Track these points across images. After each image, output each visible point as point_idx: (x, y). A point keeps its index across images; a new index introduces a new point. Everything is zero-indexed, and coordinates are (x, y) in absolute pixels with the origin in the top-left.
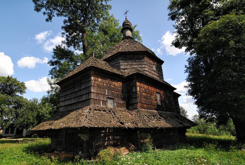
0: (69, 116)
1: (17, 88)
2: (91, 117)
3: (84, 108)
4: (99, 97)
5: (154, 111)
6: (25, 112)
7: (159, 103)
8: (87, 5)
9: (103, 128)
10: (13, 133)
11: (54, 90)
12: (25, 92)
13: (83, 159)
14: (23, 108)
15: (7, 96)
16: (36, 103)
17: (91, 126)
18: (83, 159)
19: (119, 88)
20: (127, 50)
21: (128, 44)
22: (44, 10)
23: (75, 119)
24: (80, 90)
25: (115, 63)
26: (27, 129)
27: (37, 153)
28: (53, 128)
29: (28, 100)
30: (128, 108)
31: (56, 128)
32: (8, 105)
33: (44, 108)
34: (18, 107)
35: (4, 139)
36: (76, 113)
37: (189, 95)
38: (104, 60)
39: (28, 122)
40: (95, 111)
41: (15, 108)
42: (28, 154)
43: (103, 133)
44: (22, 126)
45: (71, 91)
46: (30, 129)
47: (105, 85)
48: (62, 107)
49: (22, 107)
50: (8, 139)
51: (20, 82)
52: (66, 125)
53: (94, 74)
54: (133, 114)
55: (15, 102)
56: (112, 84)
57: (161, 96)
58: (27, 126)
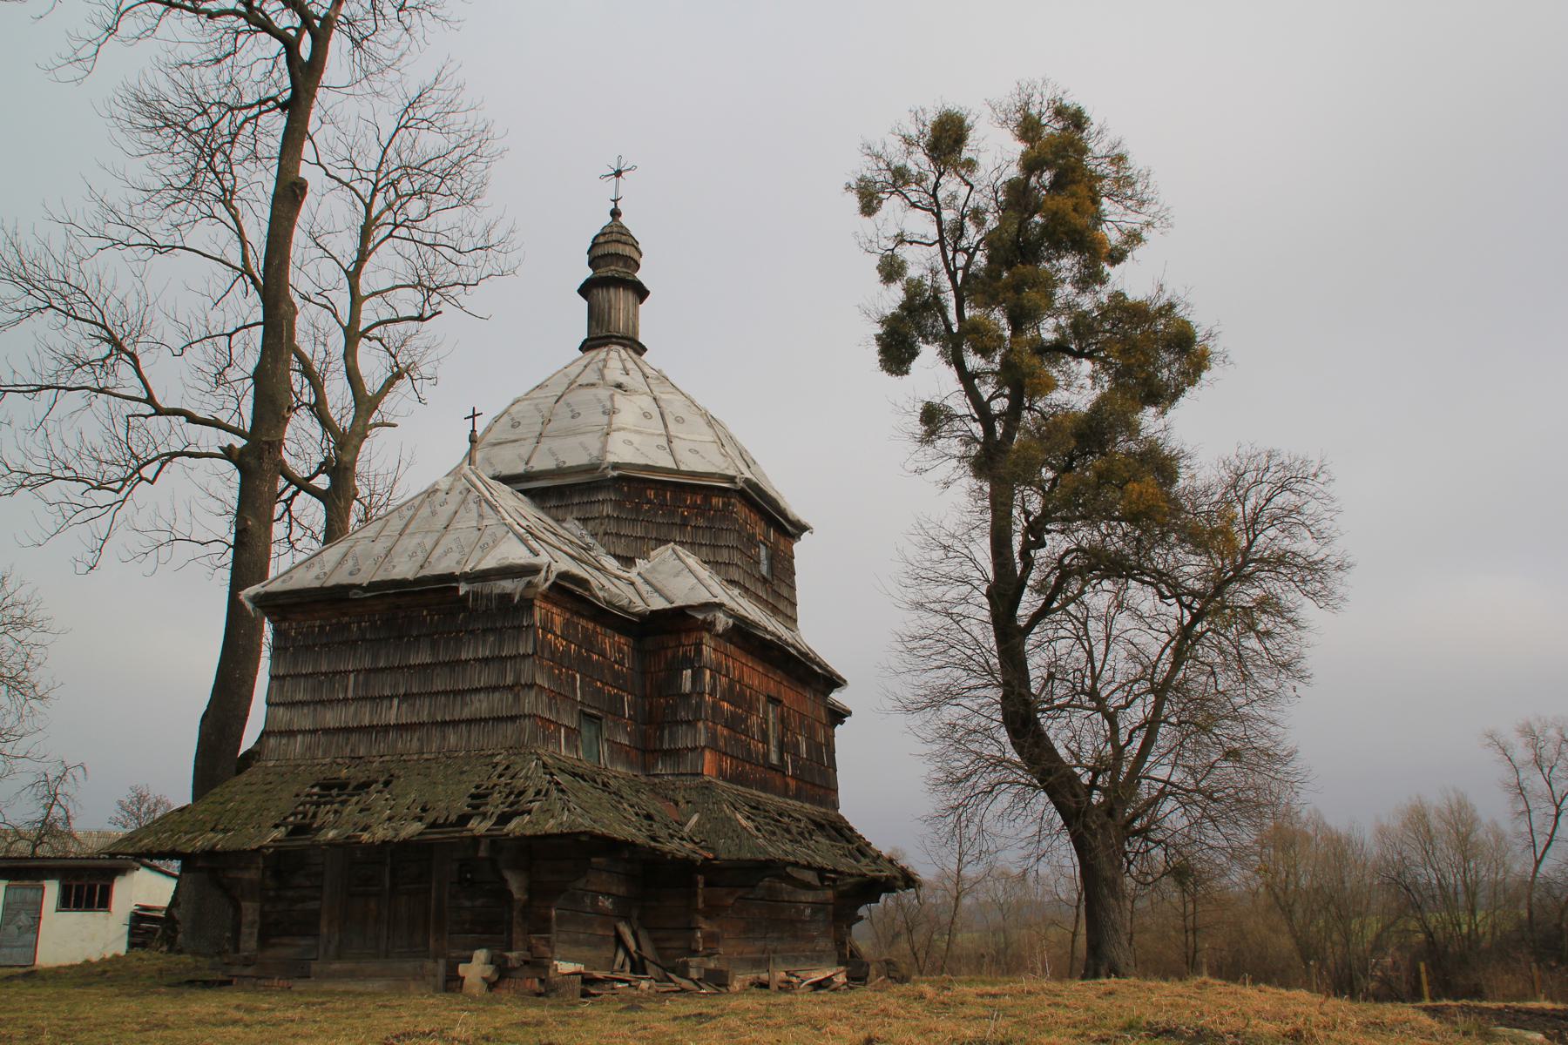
4: (558, 712)
19: (616, 666)
24: (455, 665)
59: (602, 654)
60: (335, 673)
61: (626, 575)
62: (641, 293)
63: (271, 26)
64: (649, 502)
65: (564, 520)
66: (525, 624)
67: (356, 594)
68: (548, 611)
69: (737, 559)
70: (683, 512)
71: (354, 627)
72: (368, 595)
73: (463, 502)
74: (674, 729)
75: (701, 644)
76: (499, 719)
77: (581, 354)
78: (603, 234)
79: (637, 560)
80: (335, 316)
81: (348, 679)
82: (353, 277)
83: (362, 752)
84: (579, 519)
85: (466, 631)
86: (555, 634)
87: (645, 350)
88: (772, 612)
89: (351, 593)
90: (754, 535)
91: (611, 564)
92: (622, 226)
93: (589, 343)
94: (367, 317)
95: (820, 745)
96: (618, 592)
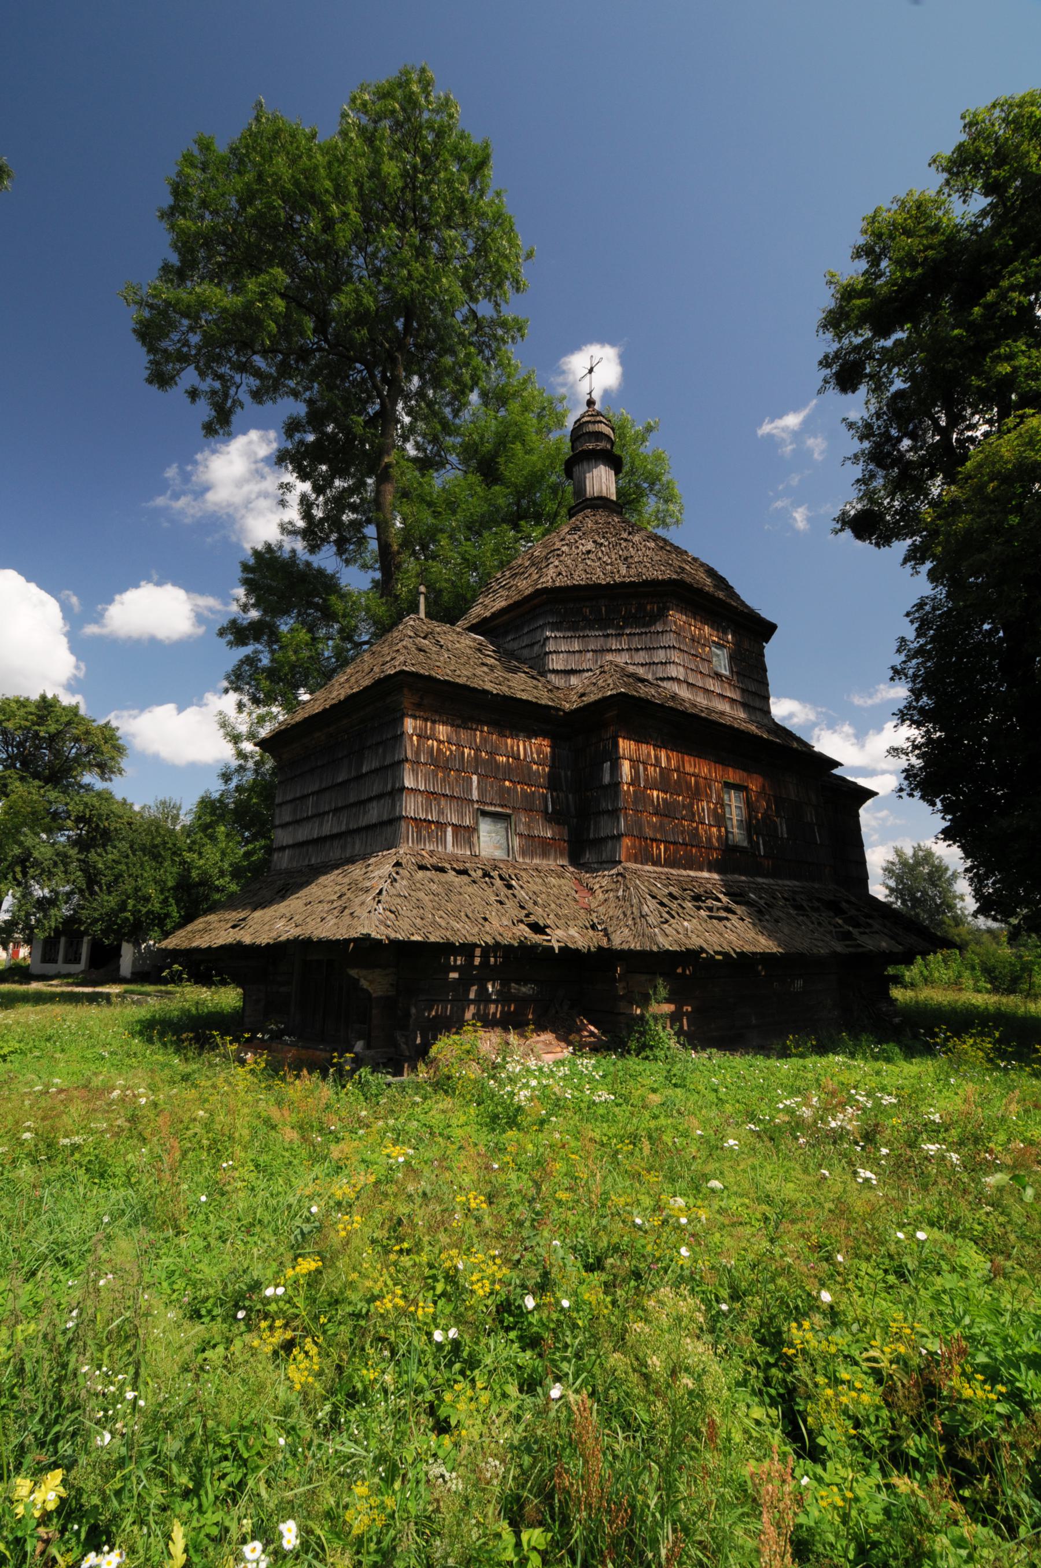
0: (313, 891)
1: (84, 750)
2: (398, 900)
3: (372, 860)
4: (441, 812)
5: (706, 874)
6: (127, 864)
7: (737, 834)
8: (400, 324)
9: (447, 948)
10: (77, 960)
11: (250, 764)
12: (120, 771)
13: (368, 1069)
14: (115, 847)
15: (40, 787)
16: (174, 823)
17: (393, 935)
18: (368, 1069)
19: (535, 767)
20: (580, 578)
21: (590, 546)
22: (189, 377)
23: (335, 904)
24: (360, 777)
25: (526, 641)
26: (137, 944)
27: (186, 1039)
28: (247, 940)
29: (137, 808)
30: (576, 859)
31: (258, 941)
32: (49, 831)
33: (208, 849)
34: (94, 838)
35: (35, 986)
36: (339, 879)
37: (911, 795)
38: (473, 628)
39: (140, 911)
40: (420, 874)
41: (82, 844)
42: (153, 1043)
43: (455, 968)
44: (114, 931)
46: (151, 942)
48: (282, 849)
49: (110, 840)
50: (56, 987)
51: (95, 724)
52: (298, 929)
53: (419, 706)
54: (596, 886)
55: (79, 819)
56: (503, 750)
57: (749, 804)
58: (136, 932)
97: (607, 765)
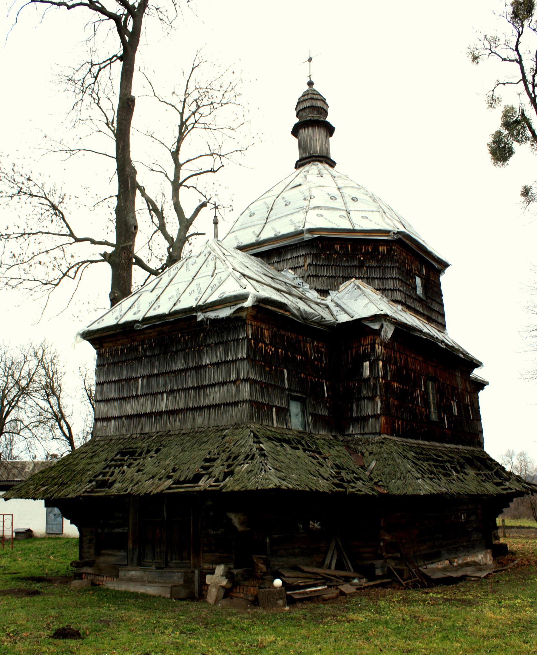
4: (270, 397)
24: (199, 368)
45: (152, 367)
47: (282, 353)
59: (305, 354)
60: (131, 379)
61: (323, 302)
62: (330, 130)
63: (104, 10)
64: (336, 252)
65: (282, 270)
66: (241, 337)
67: (138, 326)
68: (258, 328)
69: (398, 284)
70: (360, 258)
71: (140, 348)
72: (145, 326)
73: (206, 261)
74: (360, 403)
75: (375, 343)
76: (227, 405)
77: (295, 170)
78: (303, 96)
79: (330, 292)
80: (166, 176)
81: (138, 382)
82: (175, 154)
83: (147, 430)
84: (291, 269)
85: (205, 346)
86: (264, 342)
87: (335, 164)
88: (427, 320)
89: (135, 326)
90: (411, 270)
91: (313, 295)
92: (314, 90)
93: (299, 163)
94: (183, 175)
95: (468, 405)
96: (313, 311)
97: (367, 364)
